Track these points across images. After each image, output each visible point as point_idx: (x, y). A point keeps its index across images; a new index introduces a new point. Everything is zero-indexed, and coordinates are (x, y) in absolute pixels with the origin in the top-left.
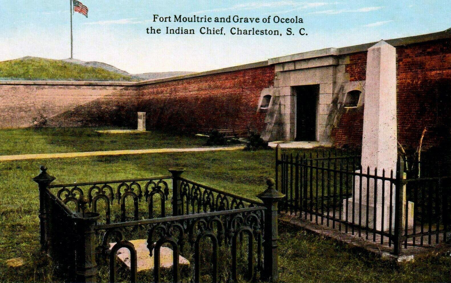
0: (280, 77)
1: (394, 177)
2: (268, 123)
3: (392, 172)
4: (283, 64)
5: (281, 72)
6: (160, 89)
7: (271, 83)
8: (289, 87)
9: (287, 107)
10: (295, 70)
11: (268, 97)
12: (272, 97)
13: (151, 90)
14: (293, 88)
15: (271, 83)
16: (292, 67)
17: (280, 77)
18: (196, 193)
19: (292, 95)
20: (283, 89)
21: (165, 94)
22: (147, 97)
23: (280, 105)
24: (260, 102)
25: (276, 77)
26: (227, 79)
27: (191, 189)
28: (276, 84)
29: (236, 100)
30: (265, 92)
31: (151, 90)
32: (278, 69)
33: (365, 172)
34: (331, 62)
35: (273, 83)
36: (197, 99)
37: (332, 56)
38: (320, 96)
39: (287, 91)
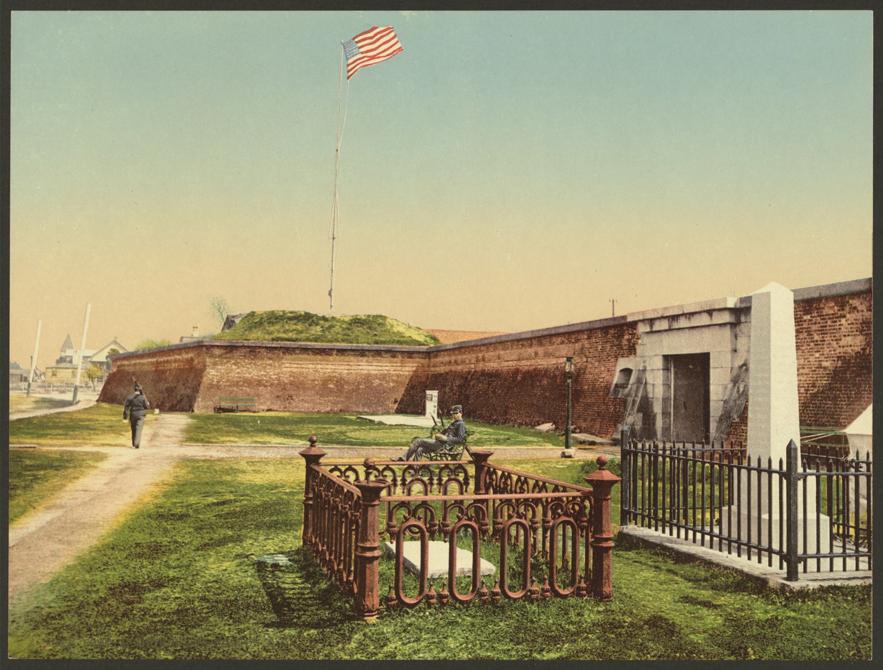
0: (645, 340)
1: (785, 468)
2: (29, 385)
3: (781, 462)
4: (651, 321)
5: (648, 333)
6: (459, 358)
7: (632, 350)
8: (661, 357)
9: (658, 384)
10: (670, 330)
11: (627, 372)
12: (634, 372)
13: (447, 359)
14: (666, 358)
15: (632, 350)
16: (704, 320)
17: (645, 340)
18: (505, 483)
19: (666, 369)
20: (650, 359)
21: (468, 363)
22: (442, 369)
23: (646, 383)
24: (617, 379)
25: (640, 341)
26: (563, 343)
27: (514, 484)
28: (639, 349)
29: (577, 376)
30: (623, 363)
31: (447, 359)
32: (642, 328)
33: (754, 464)
34: (727, 318)
35: (635, 349)
36: (517, 371)
37: (730, 310)
38: (711, 371)
39: (659, 363)
